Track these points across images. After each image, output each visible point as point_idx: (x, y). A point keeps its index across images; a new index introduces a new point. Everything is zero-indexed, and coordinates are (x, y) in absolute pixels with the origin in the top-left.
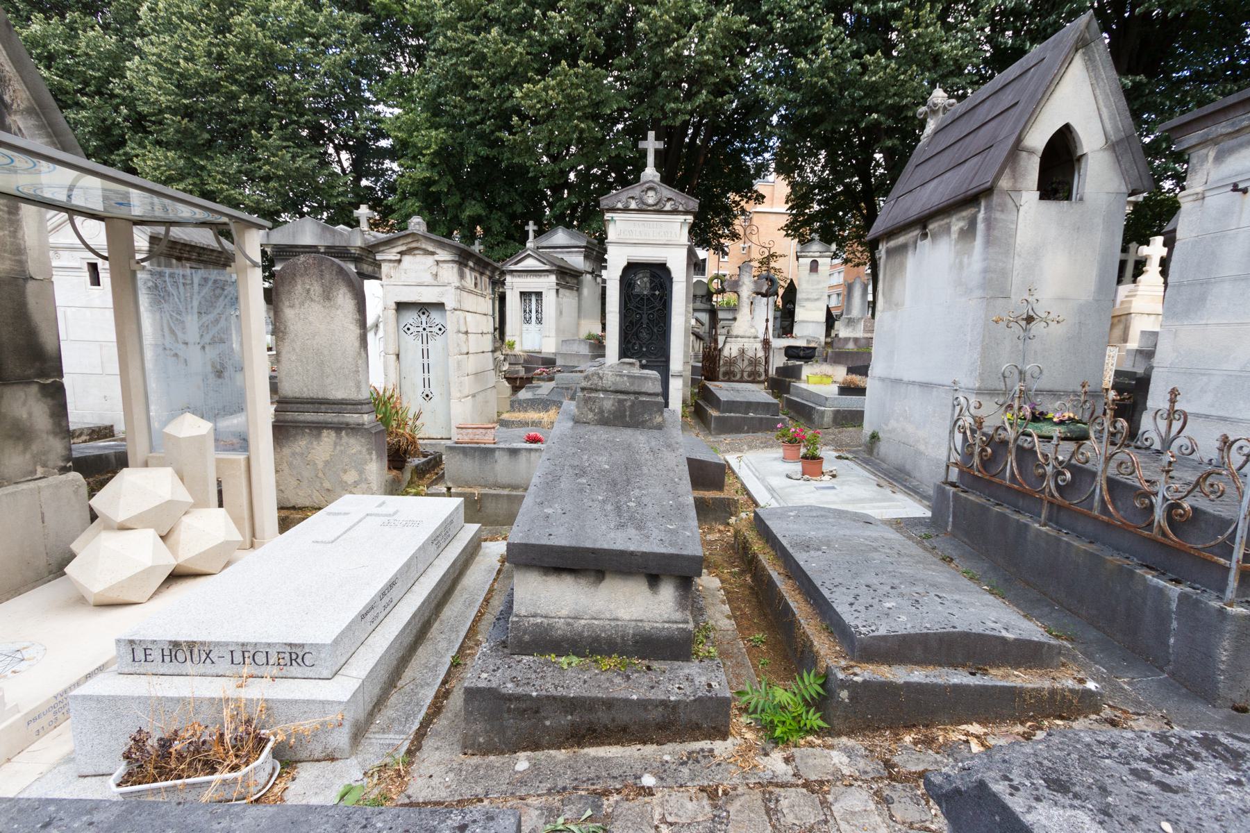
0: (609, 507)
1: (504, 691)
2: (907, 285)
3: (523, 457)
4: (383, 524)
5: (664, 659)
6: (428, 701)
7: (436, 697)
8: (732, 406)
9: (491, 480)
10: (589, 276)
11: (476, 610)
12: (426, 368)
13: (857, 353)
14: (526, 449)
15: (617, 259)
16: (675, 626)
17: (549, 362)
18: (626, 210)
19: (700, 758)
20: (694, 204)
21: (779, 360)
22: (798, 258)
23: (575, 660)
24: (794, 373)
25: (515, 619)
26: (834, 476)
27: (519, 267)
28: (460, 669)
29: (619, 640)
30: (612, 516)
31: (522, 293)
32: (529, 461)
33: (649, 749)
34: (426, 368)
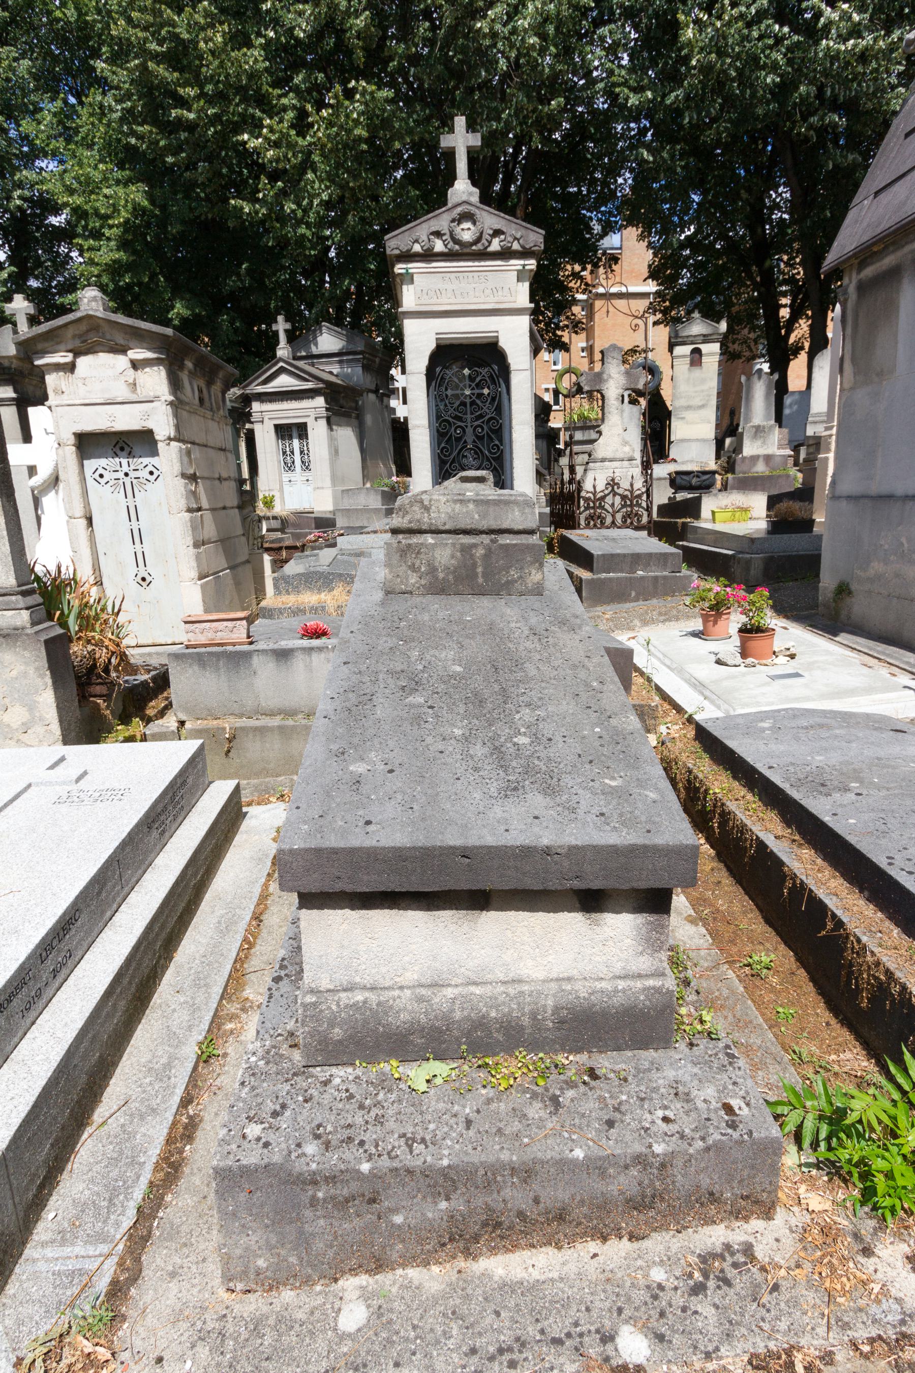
0: (479, 750)
1: (299, 1166)
2: (901, 337)
3: (299, 663)
4: (58, 802)
5: (618, 1049)
6: (154, 1152)
7: (169, 1141)
8: (613, 561)
9: (250, 704)
10: (372, 397)
11: (239, 938)
12: (137, 537)
13: (770, 477)
14: (304, 649)
15: (419, 340)
16: (639, 984)
17: (325, 523)
18: (428, 256)
19: (731, 1273)
20: (535, 238)
21: (662, 495)
22: (671, 350)
23: (441, 1069)
24: (693, 508)
25: (310, 999)
26: (792, 656)
27: (270, 387)
28: (215, 1063)
29: (526, 1021)
30: (488, 768)
31: (277, 427)
32: (309, 668)
33: (617, 1250)
34: (137, 537)
